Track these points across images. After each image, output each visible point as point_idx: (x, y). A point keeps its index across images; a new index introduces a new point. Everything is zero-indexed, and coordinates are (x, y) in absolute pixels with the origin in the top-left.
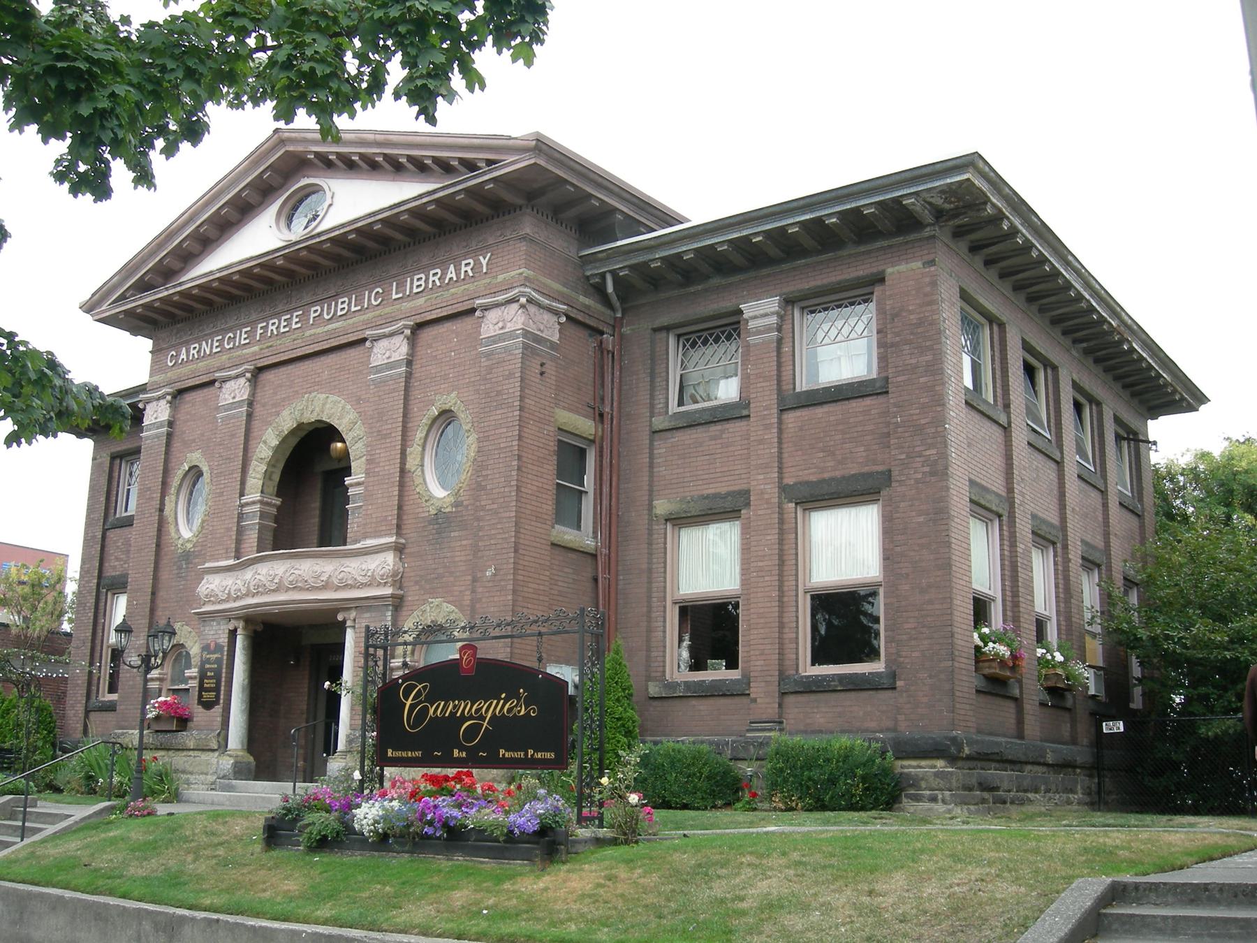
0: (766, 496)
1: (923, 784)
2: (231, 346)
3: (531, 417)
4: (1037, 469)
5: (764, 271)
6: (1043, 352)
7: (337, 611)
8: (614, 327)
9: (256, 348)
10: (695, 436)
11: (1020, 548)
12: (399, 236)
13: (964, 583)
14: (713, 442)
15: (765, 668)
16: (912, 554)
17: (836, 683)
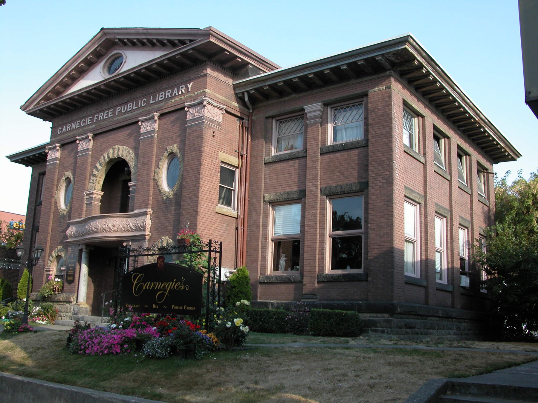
0: (313, 193)
1: (379, 325)
2: (84, 125)
3: (207, 155)
4: (439, 183)
5: (315, 91)
6: (443, 131)
7: (123, 241)
8: (249, 116)
9: (94, 126)
10: (283, 165)
11: (429, 218)
12: (153, 75)
13: (401, 234)
14: (291, 168)
15: (310, 270)
16: (377, 219)
17: (342, 278)
